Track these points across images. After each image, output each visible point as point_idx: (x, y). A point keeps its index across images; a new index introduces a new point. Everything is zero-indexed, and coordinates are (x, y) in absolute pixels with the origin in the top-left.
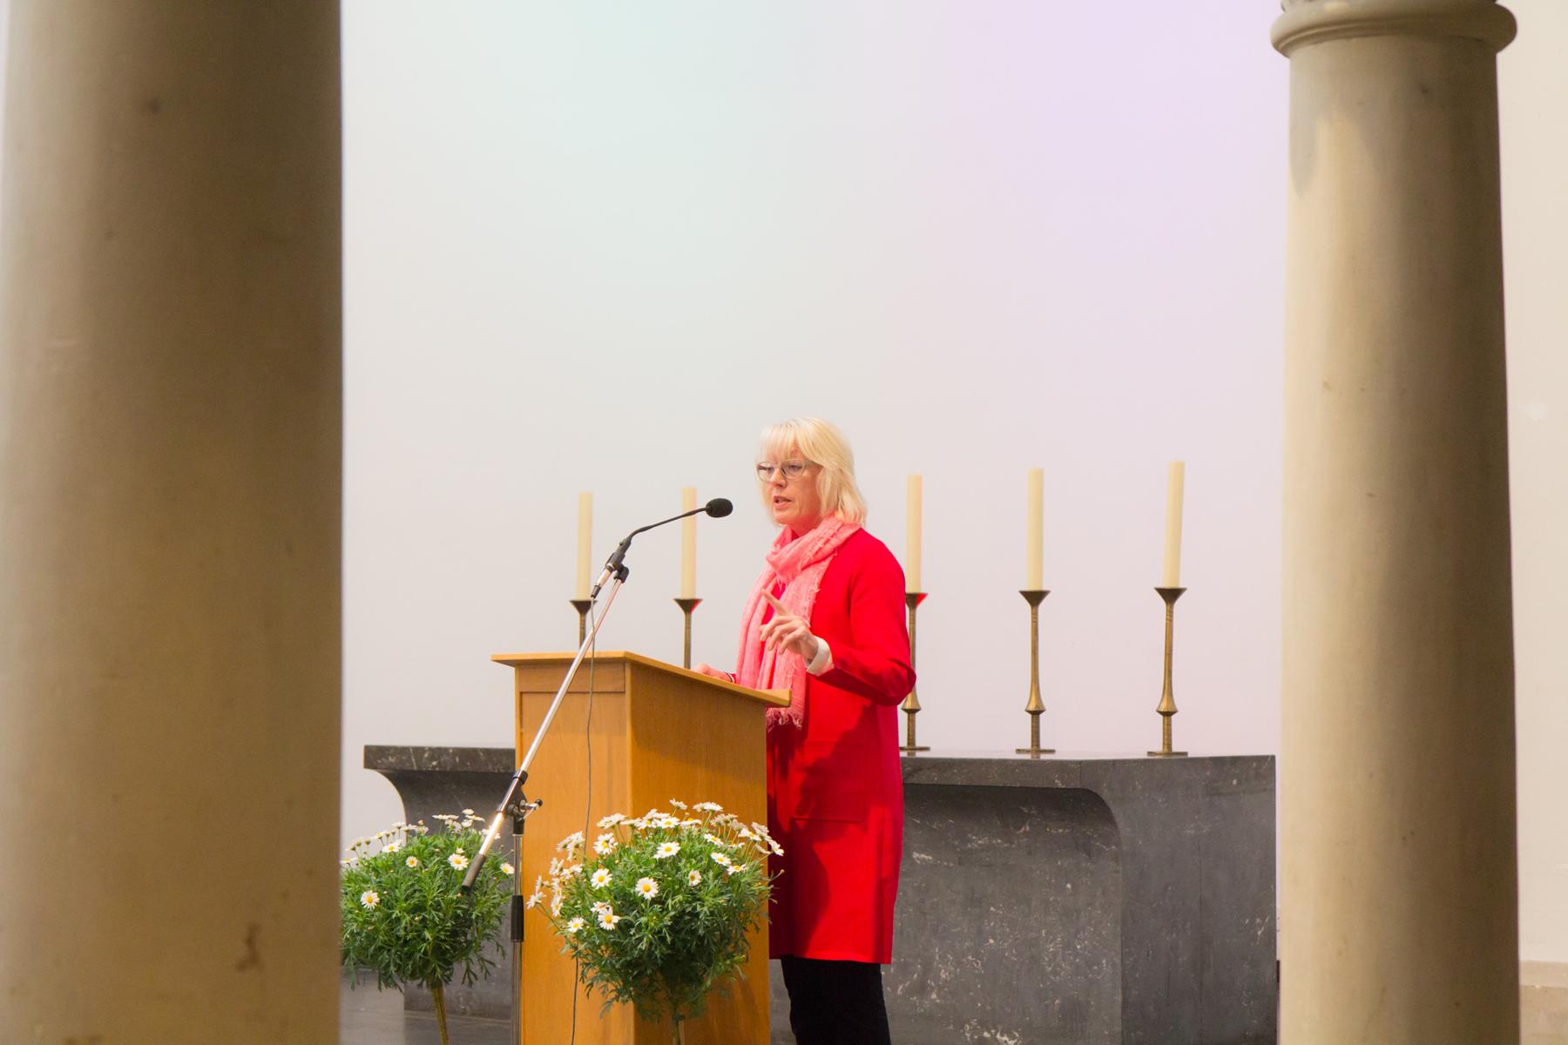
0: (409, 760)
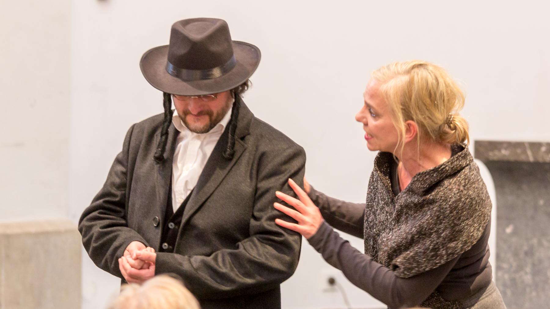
0: (525, 152)
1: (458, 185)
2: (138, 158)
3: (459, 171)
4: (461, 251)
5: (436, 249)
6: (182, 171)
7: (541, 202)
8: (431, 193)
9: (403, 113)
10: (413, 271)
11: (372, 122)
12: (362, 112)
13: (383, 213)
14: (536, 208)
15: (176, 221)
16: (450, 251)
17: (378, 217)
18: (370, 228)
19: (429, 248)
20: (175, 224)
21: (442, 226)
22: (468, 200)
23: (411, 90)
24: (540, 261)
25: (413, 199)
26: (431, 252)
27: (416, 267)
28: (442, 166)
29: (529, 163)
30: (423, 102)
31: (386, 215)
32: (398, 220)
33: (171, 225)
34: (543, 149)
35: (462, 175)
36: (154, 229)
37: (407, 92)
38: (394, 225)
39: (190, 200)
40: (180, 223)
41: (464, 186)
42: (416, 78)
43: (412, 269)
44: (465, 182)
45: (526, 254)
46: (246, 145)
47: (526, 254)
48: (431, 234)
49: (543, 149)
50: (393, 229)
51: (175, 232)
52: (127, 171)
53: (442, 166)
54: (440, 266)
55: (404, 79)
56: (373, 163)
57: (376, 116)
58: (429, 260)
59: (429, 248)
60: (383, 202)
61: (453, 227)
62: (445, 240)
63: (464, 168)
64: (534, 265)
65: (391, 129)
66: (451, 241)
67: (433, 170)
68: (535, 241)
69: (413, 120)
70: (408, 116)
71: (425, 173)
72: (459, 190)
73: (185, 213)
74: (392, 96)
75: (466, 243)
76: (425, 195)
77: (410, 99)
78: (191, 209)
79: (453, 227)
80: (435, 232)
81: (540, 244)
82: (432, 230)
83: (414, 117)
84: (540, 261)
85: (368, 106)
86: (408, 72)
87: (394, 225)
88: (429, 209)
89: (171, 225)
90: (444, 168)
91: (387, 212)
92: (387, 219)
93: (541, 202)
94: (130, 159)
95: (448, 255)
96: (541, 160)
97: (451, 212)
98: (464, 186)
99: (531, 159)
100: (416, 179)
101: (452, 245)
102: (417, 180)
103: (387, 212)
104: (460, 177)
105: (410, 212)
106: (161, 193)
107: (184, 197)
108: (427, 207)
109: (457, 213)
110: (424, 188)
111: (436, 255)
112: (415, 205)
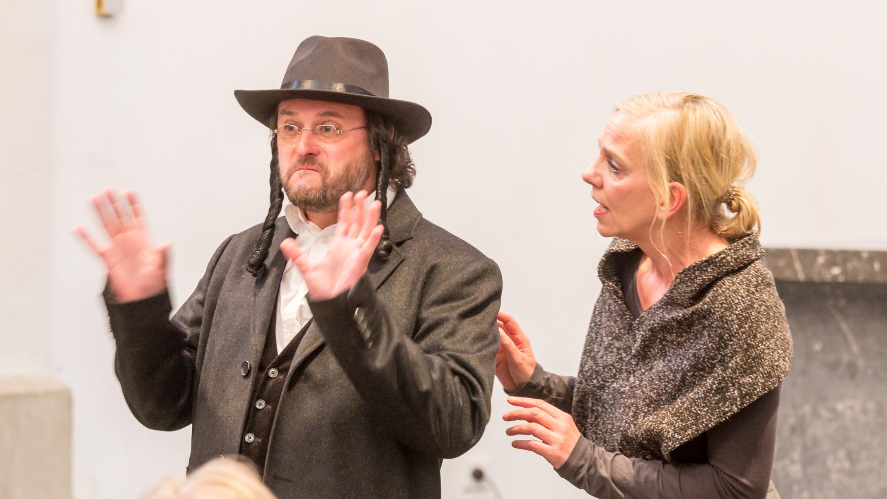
0: (790, 265)
1: (747, 285)
2: (228, 277)
3: (746, 266)
4: (764, 389)
5: (722, 388)
6: (297, 292)
7: (817, 347)
8: (704, 296)
9: (668, 166)
10: (689, 432)
11: (612, 182)
12: (597, 166)
13: (611, 352)
14: (809, 356)
15: (281, 367)
16: (744, 391)
17: (600, 361)
18: (586, 381)
19: (712, 389)
20: (280, 372)
21: (728, 351)
22: (763, 307)
23: (683, 133)
24: (816, 442)
25: (674, 314)
26: (714, 395)
27: (692, 424)
28: (720, 254)
29: (797, 283)
30: (700, 153)
31: (618, 354)
32: (644, 355)
33: (273, 373)
34: (821, 260)
35: (751, 270)
36: (242, 380)
37: (676, 135)
38: (637, 365)
39: (307, 333)
40: (287, 369)
41: (756, 286)
42: (691, 116)
43: (685, 429)
44: (757, 281)
45: (793, 430)
46: (404, 254)
47: (793, 430)
48: (714, 365)
49: (821, 260)
50: (634, 371)
51: (278, 384)
52: (204, 300)
53: (720, 254)
54: (732, 417)
55: (671, 117)
56: (597, 274)
57: (619, 170)
58: (713, 409)
59: (712, 389)
60: (610, 338)
61: (747, 350)
62: (735, 373)
63: (753, 261)
64: (805, 448)
65: (646, 193)
66: (745, 373)
67: (706, 261)
68: (807, 409)
69: (681, 181)
70: (675, 175)
71: (694, 267)
72: (748, 291)
73: (298, 352)
74: (652, 138)
75: (769, 375)
76: (692, 305)
77: (681, 145)
78: (309, 346)
79: (747, 350)
80: (720, 361)
81: (815, 414)
82: (713, 359)
83: (684, 176)
84: (816, 442)
85: (608, 156)
86: (680, 106)
87: (637, 365)
88: (704, 327)
89: (273, 373)
90: (722, 259)
91: (618, 349)
92: (621, 359)
93: (817, 347)
94: (212, 280)
95: (743, 397)
96: (816, 278)
97: (741, 327)
98: (756, 286)
99: (801, 277)
100: (678, 280)
101: (747, 380)
102: (680, 282)
103: (618, 349)
104: (748, 273)
105: (669, 338)
106: (259, 322)
107: (297, 330)
108: (700, 323)
109: (750, 327)
110: (692, 291)
111: (724, 399)
112: (679, 323)
